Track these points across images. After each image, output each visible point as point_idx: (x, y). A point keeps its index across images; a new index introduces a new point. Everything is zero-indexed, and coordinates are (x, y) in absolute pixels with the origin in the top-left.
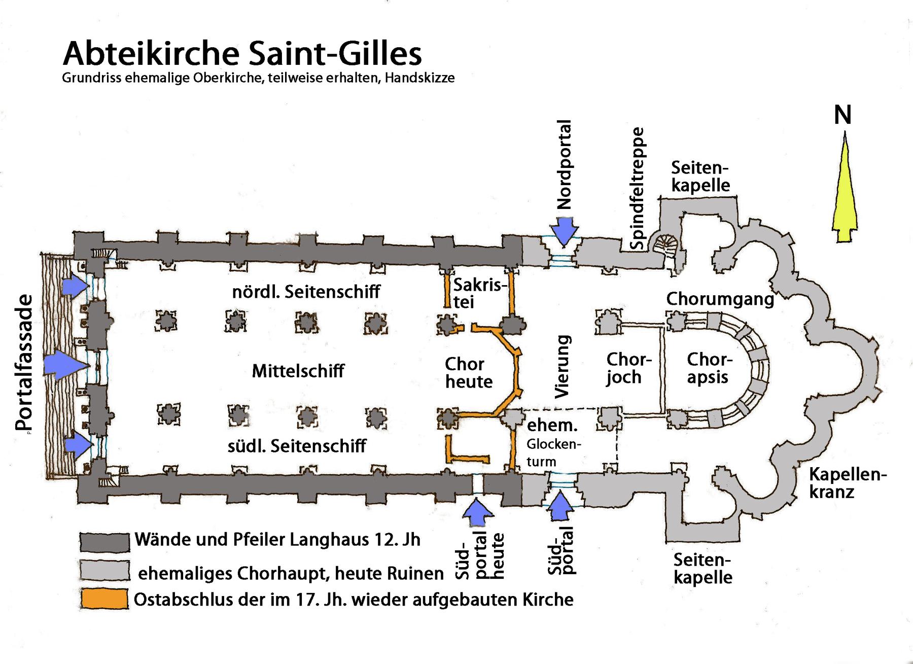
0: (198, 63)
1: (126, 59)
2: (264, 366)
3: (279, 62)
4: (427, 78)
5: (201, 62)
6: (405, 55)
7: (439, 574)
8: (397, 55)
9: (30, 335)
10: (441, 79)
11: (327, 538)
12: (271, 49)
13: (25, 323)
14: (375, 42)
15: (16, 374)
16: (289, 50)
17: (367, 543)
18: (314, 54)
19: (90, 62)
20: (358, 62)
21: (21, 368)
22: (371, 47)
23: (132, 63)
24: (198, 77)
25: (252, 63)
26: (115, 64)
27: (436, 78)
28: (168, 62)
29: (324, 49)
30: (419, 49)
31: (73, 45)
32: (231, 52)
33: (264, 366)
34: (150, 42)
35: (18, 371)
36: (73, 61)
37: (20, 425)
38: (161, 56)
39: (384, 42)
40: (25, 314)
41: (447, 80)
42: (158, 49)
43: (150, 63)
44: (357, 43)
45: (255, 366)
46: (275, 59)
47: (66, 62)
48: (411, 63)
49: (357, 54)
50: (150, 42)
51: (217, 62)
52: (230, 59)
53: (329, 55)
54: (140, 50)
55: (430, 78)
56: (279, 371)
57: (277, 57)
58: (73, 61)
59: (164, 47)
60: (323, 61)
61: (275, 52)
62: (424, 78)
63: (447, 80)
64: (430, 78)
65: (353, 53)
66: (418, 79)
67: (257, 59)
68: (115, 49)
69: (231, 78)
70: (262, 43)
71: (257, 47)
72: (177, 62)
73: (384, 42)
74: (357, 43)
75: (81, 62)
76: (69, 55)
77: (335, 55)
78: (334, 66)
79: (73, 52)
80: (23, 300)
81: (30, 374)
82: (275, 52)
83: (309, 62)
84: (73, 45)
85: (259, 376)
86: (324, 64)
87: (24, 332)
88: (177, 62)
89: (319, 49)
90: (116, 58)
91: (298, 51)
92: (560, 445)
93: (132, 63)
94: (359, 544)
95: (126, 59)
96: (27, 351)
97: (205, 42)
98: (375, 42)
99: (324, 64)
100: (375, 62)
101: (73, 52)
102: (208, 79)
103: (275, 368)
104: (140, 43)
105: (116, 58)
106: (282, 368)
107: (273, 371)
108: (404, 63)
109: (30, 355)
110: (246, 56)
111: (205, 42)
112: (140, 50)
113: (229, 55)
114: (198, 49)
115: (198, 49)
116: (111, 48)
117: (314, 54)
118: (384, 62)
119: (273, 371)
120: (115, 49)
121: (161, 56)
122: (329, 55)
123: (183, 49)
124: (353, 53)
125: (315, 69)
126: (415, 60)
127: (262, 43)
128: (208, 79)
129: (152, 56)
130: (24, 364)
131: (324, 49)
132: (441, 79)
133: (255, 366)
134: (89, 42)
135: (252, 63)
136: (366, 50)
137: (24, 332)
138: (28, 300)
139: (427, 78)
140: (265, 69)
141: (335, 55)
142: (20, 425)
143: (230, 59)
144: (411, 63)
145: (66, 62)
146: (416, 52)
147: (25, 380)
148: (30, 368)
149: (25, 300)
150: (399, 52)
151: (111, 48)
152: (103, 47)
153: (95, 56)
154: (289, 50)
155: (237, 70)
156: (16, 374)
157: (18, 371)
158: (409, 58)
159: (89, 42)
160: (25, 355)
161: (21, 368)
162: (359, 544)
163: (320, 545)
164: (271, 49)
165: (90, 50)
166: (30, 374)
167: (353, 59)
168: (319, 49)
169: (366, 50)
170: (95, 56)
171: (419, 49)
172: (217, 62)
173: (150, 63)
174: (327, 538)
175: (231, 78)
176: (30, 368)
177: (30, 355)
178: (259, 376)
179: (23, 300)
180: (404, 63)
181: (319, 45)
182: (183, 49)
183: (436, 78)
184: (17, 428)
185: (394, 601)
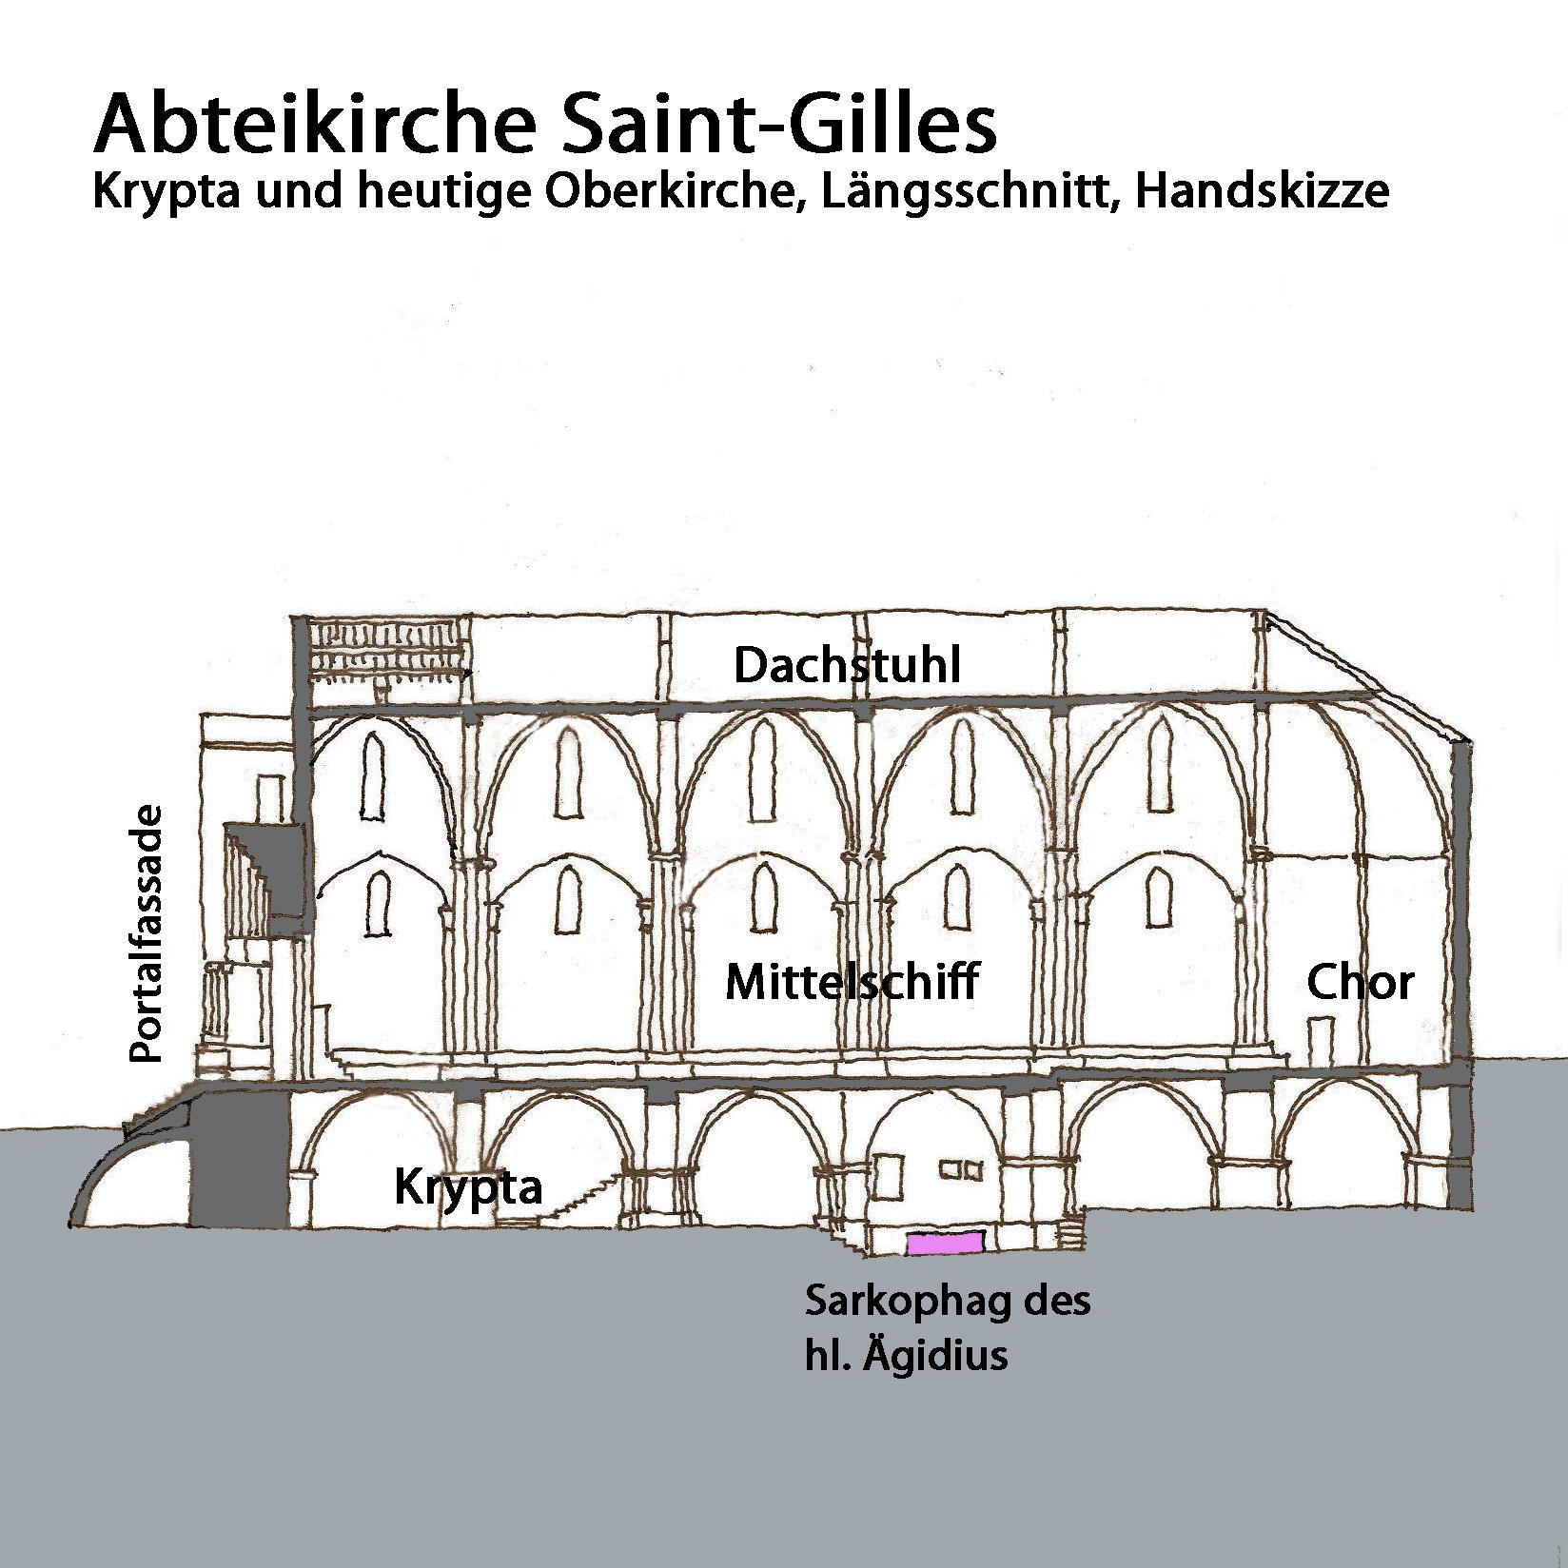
0: (434, 148)
1: (253, 138)
2: (757, 969)
3: (639, 145)
4: (1289, 193)
5: (443, 144)
6: (953, 126)
7: (269, 197)
8: (929, 129)
9: (157, 881)
10: (1340, 194)
11: (910, 1352)
12: (617, 113)
13: (147, 860)
14: (881, 95)
15: (132, 956)
16: (663, 115)
17: (1005, 1363)
18: (726, 125)
19: (161, 144)
20: (836, 145)
21: (140, 943)
22: (869, 107)
23: (268, 148)
24: (563, 189)
25: (568, 147)
26: (226, 149)
27: (1320, 192)
28: (357, 146)
29: (752, 112)
30: (990, 112)
31: (119, 101)
32: (516, 120)
33: (757, 969)
34: (313, 95)
35: (135, 950)
36: (119, 142)
37: (139, 1052)
38: (342, 129)
39: (904, 95)
40: (150, 840)
41: (1360, 197)
42: (334, 113)
43: (312, 147)
44: (835, 96)
45: (734, 969)
46: (628, 138)
47: (100, 146)
48: (971, 148)
49: (836, 126)
50: (313, 95)
51: (481, 146)
52: (513, 138)
53: (763, 128)
54: (290, 115)
55: (1302, 193)
56: (798, 984)
57: (633, 131)
58: (119, 142)
59: (349, 106)
60: (748, 143)
61: (628, 119)
62: (1277, 191)
63: (1360, 197)
64: (1302, 193)
65: (823, 123)
66: (1258, 197)
67: (584, 137)
68: (227, 112)
69: (682, 193)
70: (595, 96)
71: (583, 107)
72: (381, 146)
73: (904, 95)
74: (835, 96)
75: (138, 146)
76: (108, 129)
77: (780, 128)
78: (774, 158)
79: (119, 121)
80: (145, 815)
81: (158, 956)
82: (628, 119)
83: (714, 146)
84: (119, 101)
85: (745, 994)
86: (751, 149)
87: (147, 875)
88: (381, 146)
89: (739, 111)
90: (226, 136)
91: (687, 116)
92: (884, 1302)
93: (268, 148)
94: (983, 1366)
95: (253, 138)
96: (151, 912)
97: (452, 95)
98: (881, 95)
99: (751, 149)
100: (881, 146)
101: (119, 121)
102: (598, 194)
103: (789, 974)
104: (290, 97)
105: (226, 136)
106: (808, 974)
107: (782, 982)
108: (952, 148)
109: (157, 920)
110: (554, 129)
111: (452, 95)
112: (290, 115)
113: (510, 127)
114: (434, 112)
115: (434, 112)
116: (214, 110)
117: (726, 125)
118: (904, 146)
119: (782, 982)
120: (227, 112)
121: (342, 129)
122: (763, 128)
123: (395, 112)
124: (823, 123)
125: (727, 164)
126: (980, 140)
127: (595, 96)
128: (598, 194)
129: (319, 129)
130: (147, 936)
131: (752, 112)
132: (1340, 194)
133: (734, 969)
134: (159, 95)
135: (568, 147)
136: (858, 115)
137: (147, 875)
138: (154, 815)
139: (1289, 193)
140: (609, 166)
141: (780, 128)
142: (139, 1052)
143: (513, 138)
144: (971, 148)
145: (100, 146)
146: (983, 120)
147: (147, 967)
148: (157, 943)
149: (149, 816)
150: (940, 120)
151: (214, 110)
152: (197, 107)
153: (175, 131)
154: (663, 115)
155: (533, 169)
156: (132, 956)
157: (135, 950)
158: (966, 136)
159: (159, 95)
160: (147, 919)
161: (140, 943)
162: (983, 1366)
163: (893, 1370)
164: (617, 113)
165: (161, 116)
166: (158, 956)
167: (824, 137)
168: (739, 111)
169: (858, 115)
170: (175, 131)
171: (990, 112)
172: (481, 146)
173: (312, 147)
174: (910, 1352)
175: (682, 193)
176: (157, 943)
177: (157, 920)
178: (745, 994)
179: (145, 815)
180: (952, 148)
181: (739, 103)
182: (395, 112)
183: (1320, 192)
184: (133, 1059)
185: (1055, 1304)
